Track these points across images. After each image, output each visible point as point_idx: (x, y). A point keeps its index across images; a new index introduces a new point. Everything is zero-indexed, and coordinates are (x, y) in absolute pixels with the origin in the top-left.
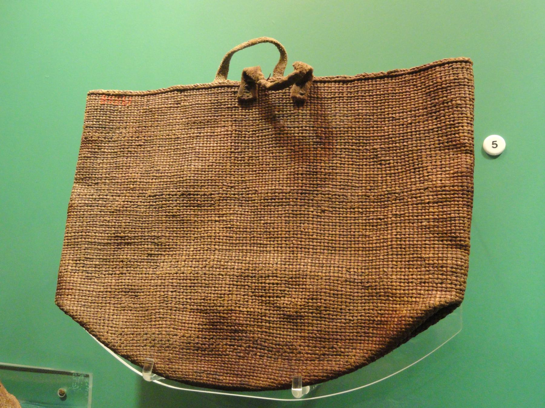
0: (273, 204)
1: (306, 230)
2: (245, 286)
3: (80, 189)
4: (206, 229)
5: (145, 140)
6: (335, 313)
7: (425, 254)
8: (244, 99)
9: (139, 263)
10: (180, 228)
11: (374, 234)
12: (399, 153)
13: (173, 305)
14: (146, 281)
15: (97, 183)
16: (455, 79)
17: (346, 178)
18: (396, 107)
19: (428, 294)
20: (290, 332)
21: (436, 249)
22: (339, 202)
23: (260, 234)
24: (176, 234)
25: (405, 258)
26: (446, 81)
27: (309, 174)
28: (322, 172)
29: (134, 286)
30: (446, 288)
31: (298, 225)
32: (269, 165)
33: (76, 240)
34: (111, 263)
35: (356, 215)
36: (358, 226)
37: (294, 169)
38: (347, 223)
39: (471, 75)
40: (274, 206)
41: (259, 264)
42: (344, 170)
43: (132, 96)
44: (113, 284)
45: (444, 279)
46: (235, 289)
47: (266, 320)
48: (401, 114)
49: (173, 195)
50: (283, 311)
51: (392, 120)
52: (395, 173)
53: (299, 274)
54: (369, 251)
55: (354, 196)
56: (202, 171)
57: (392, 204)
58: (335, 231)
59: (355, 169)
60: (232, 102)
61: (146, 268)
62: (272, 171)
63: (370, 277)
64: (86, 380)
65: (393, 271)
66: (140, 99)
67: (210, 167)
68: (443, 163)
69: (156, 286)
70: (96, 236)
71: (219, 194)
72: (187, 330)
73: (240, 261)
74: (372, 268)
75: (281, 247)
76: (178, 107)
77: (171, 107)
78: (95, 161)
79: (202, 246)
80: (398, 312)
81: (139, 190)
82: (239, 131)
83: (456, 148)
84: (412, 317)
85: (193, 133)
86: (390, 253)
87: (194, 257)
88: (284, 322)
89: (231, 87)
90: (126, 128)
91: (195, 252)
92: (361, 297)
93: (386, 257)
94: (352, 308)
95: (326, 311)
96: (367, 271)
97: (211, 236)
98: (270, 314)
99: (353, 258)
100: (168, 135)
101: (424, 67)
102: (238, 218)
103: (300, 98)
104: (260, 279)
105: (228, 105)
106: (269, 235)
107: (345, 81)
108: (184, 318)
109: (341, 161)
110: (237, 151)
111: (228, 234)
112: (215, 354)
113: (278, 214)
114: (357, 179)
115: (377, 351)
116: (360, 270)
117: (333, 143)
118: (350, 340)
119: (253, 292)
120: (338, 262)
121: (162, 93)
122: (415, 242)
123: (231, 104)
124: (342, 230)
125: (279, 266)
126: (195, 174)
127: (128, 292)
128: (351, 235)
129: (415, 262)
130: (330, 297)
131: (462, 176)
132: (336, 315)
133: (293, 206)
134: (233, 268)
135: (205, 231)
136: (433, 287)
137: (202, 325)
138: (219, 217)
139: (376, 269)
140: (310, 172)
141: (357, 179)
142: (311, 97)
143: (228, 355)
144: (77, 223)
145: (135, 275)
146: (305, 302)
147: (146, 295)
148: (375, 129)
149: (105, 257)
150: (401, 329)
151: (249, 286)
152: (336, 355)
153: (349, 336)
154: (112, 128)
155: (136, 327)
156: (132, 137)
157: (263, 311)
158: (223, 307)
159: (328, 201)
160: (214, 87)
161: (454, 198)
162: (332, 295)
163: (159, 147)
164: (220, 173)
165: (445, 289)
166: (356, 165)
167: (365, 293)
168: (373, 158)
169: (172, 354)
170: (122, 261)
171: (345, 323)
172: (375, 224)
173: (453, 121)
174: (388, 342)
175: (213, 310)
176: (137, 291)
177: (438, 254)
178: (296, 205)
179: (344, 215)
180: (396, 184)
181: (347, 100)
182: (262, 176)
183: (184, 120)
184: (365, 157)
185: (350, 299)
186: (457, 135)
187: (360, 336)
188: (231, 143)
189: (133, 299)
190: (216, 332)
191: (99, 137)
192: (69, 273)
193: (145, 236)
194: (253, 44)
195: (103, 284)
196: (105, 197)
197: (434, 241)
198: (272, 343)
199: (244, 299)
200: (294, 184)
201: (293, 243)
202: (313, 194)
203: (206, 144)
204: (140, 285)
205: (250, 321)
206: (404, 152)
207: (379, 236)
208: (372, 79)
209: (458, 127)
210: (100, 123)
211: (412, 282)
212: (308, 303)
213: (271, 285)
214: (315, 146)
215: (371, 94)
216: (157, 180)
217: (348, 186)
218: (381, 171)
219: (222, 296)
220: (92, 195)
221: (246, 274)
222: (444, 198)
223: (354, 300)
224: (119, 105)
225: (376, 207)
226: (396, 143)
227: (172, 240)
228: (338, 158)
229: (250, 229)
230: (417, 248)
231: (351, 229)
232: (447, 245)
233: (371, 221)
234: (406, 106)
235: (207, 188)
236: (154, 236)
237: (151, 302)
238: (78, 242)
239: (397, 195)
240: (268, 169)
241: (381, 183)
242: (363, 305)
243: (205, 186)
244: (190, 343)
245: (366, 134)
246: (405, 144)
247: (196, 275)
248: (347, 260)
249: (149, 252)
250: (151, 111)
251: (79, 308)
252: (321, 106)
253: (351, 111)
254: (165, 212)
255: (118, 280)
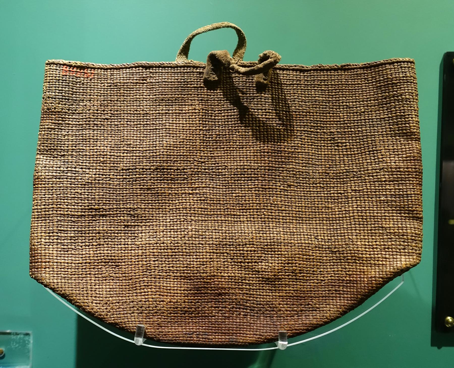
0: (243, 179)
1: (275, 203)
2: (224, 253)
3: (43, 160)
4: (180, 201)
5: (112, 114)
6: (308, 275)
7: (385, 224)
8: (210, 80)
9: (116, 235)
10: (155, 201)
11: (335, 206)
12: (354, 137)
13: (156, 273)
14: (126, 251)
15: (64, 155)
16: (403, 77)
17: (307, 156)
18: (349, 97)
19: (393, 258)
20: (269, 293)
21: (396, 220)
22: (303, 178)
23: (233, 206)
24: (151, 206)
25: (367, 227)
26: (396, 77)
27: (274, 153)
28: (285, 151)
29: (114, 256)
30: (409, 253)
31: (268, 198)
32: (236, 143)
33: (47, 213)
34: (87, 235)
35: (318, 190)
36: (321, 199)
37: (260, 147)
38: (311, 197)
39: (415, 74)
40: (244, 181)
41: (235, 233)
42: (304, 150)
43: (94, 68)
44: (92, 255)
45: (406, 245)
46: (215, 257)
47: (246, 283)
48: (354, 104)
49: (146, 169)
50: (262, 275)
51: (346, 108)
52: (351, 155)
53: (274, 242)
54: (333, 220)
55: (315, 173)
56: (174, 147)
57: (351, 181)
58: (301, 204)
59: (314, 149)
60: (198, 82)
61: (124, 239)
62: (240, 148)
63: (337, 243)
64: (27, 338)
65: (357, 239)
66: (103, 73)
67: (181, 143)
68: (395, 147)
69: (138, 256)
70: (68, 208)
71: (190, 169)
72: (173, 296)
73: (216, 231)
74: (338, 236)
75: (253, 218)
76: (145, 83)
77: (137, 83)
78: (59, 133)
79: (178, 217)
80: (366, 273)
81: (110, 163)
82: (206, 110)
83: (407, 136)
84: (382, 278)
85: (162, 110)
86: (353, 223)
87: (172, 228)
88: (263, 284)
89: (197, 67)
90: (90, 101)
91: (172, 223)
92: (330, 260)
93: (349, 226)
94: (322, 270)
95: (300, 273)
96: (333, 238)
97: (186, 208)
98: (250, 278)
99: (318, 227)
100: (137, 111)
101: (375, 64)
102: (211, 192)
103: (263, 83)
104: (238, 246)
105: (194, 84)
106: (242, 207)
107: (302, 71)
108: (168, 285)
109: (302, 142)
110: (204, 128)
111: (202, 206)
112: (202, 316)
113: (249, 188)
114: (317, 158)
115: (349, 306)
116: (326, 238)
117: (294, 125)
118: (323, 297)
119: (232, 259)
120: (306, 230)
121: (126, 68)
122: (375, 214)
123: (197, 84)
124: (307, 203)
125: (254, 235)
126: (168, 150)
127: (108, 262)
128: (315, 207)
129: (377, 231)
130: (303, 261)
131: (414, 160)
132: (310, 277)
133: (262, 181)
134: (212, 238)
135: (180, 203)
136: (397, 252)
137: (187, 291)
138: (192, 190)
139: (341, 236)
140: (275, 150)
141: (317, 158)
142: (271, 82)
143: (214, 316)
144: (46, 196)
145: (113, 246)
146: (281, 266)
147: (128, 265)
148: (331, 114)
149: (80, 229)
150: (372, 287)
151: (228, 254)
152: (312, 311)
153: (321, 294)
154: (76, 100)
155: (121, 295)
156: (97, 110)
157: (243, 275)
158: (206, 273)
159: (293, 177)
160: (181, 67)
161: (409, 178)
162: (305, 260)
163: (127, 122)
164: (191, 149)
165: (408, 254)
166: (315, 146)
167: (333, 257)
168: (330, 140)
169: (160, 319)
170: (99, 233)
171: (317, 283)
172: (337, 198)
173: (404, 113)
174: (360, 299)
175: (197, 276)
176: (118, 261)
177: (397, 224)
178: (265, 180)
179: (308, 190)
180: (353, 164)
181: (304, 87)
182: (230, 153)
183: (151, 96)
184: (323, 139)
185: (321, 262)
186: (407, 125)
187: (332, 294)
188: (199, 121)
189: (114, 269)
190: (201, 297)
191: (62, 109)
192: (43, 246)
193: (120, 209)
194: (217, 28)
195: (81, 256)
196: (73, 169)
197: (392, 213)
198: (253, 303)
199: (224, 265)
200: (261, 161)
201: (264, 214)
202: (279, 170)
203: (176, 121)
204: (120, 255)
205: (231, 285)
206: (359, 137)
207: (341, 209)
208: (327, 70)
209: (407, 118)
210: (63, 94)
211: (376, 248)
212: (284, 267)
213: (249, 252)
214: (278, 127)
215: (326, 83)
216: (128, 154)
217: (309, 164)
218: (339, 152)
219: (205, 263)
220: (60, 167)
221: (225, 243)
222: (400, 178)
223: (323, 263)
224: (81, 76)
225: (336, 183)
226: (351, 129)
227: (148, 211)
228: (299, 139)
229: (223, 201)
230: (377, 219)
231: (315, 201)
232: (405, 217)
233: (332, 195)
234: (358, 97)
235: (180, 163)
236: (130, 208)
237: (134, 272)
238: (49, 215)
239: (354, 173)
240: (235, 146)
241: (339, 162)
242: (332, 267)
243: (178, 161)
244: (177, 308)
245: (323, 119)
246: (360, 129)
247: (176, 245)
248: (313, 228)
249: (126, 223)
250: (116, 86)
251: (59, 281)
252: (281, 91)
253: (308, 97)
254: (140, 186)
255: (96, 251)
